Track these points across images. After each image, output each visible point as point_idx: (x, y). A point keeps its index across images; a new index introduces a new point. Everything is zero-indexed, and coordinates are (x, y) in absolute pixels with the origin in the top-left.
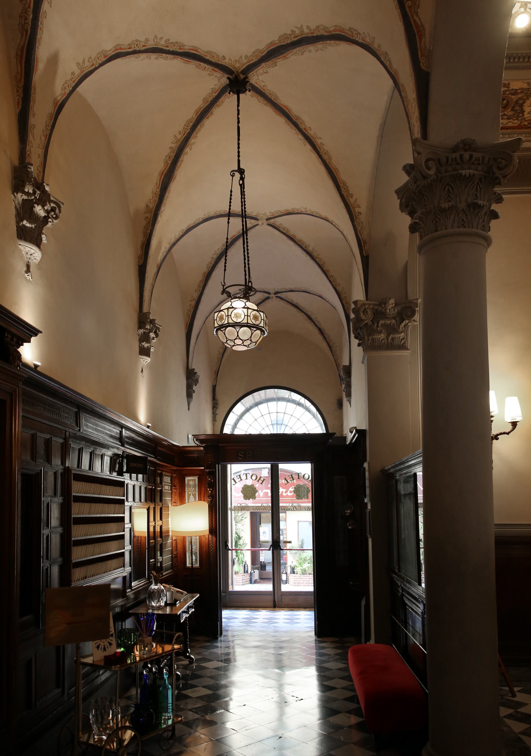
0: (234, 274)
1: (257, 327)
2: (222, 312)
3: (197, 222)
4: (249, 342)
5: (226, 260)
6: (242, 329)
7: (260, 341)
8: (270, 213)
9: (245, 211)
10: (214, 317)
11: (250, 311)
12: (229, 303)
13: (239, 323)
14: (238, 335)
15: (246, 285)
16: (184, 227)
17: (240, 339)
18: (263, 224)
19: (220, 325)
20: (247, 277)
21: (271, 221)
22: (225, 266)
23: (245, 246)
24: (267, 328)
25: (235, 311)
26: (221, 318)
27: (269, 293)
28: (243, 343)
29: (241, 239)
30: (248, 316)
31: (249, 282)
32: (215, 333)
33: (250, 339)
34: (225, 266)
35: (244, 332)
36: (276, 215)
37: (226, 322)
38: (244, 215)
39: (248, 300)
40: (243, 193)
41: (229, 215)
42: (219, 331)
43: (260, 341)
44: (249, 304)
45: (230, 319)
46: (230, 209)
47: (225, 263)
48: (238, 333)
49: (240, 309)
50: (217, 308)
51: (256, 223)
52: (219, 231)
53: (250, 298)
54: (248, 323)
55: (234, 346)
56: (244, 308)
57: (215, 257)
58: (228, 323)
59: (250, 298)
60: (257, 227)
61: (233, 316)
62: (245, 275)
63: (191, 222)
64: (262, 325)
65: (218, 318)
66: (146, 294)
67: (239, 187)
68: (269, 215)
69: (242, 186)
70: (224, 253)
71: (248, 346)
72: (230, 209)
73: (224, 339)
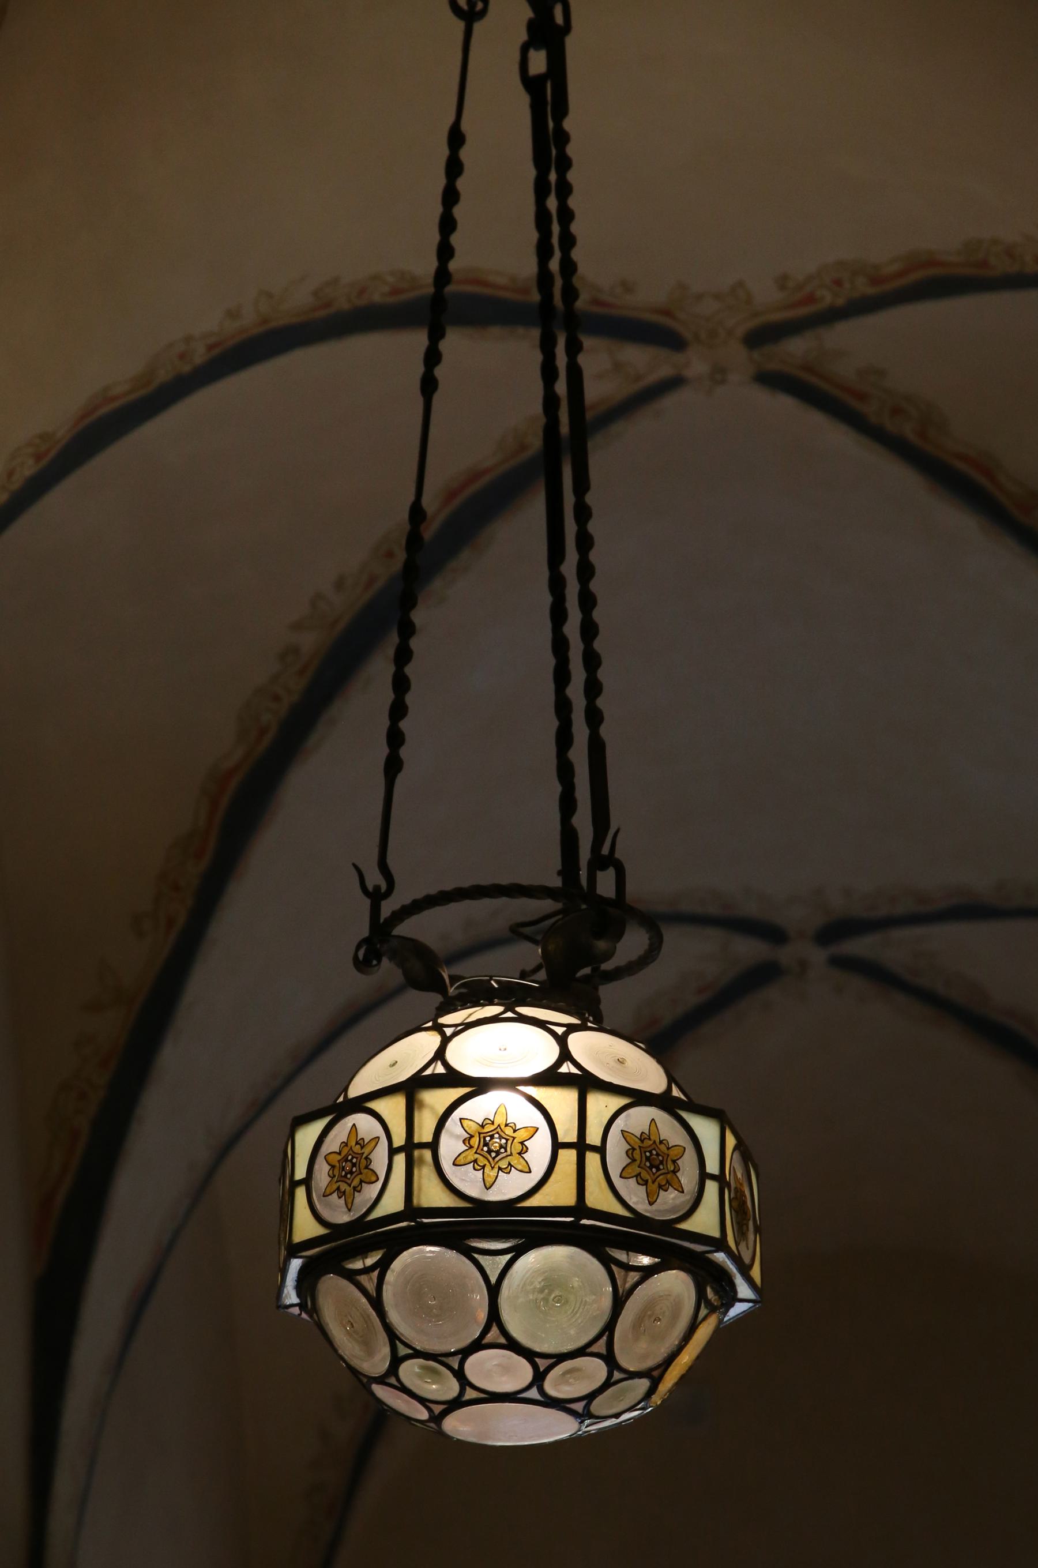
0: (468, 774)
1: (668, 1243)
2: (363, 1122)
3: (164, 375)
4: (595, 1370)
5: (401, 684)
6: (532, 1260)
7: (686, 1358)
8: (782, 282)
9: (569, 267)
10: (287, 1161)
11: (601, 1106)
12: (425, 1043)
13: (509, 1206)
14: (494, 1316)
15: (570, 889)
16: (56, 414)
17: (513, 1345)
18: (719, 374)
19: (336, 1231)
20: (583, 821)
21: (789, 351)
22: (395, 738)
23: (569, 568)
24: (752, 1249)
25: (480, 1108)
26: (352, 1167)
27: (775, 935)
28: (539, 1377)
29: (534, 510)
30: (581, 1146)
31: (599, 862)
32: (291, 1296)
33: (603, 1346)
34: (395, 738)
35: (551, 1284)
36: (827, 298)
37: (393, 1202)
38: (557, 311)
39: (591, 1015)
40: (550, 149)
41: (440, 308)
42: (333, 1288)
43: (686, 1358)
44: (593, 1049)
45: (426, 1176)
46: (445, 252)
47: (398, 710)
48: (494, 1291)
49: (511, 1083)
50: (312, 1074)
51: (665, 371)
52: (345, 443)
53: (607, 993)
54: (580, 1208)
55: (456, 1404)
56: (549, 1078)
57: (311, 642)
58: (411, 1210)
59: (607, 993)
60: (670, 402)
61: (450, 1147)
62: (568, 804)
63: (111, 369)
64: (705, 1221)
65: (322, 1170)
66: (65, 1485)
67: (523, 100)
68: (767, 298)
69: (548, 98)
70: (386, 616)
71: (580, 1408)
72: (445, 252)
73: (368, 1346)
